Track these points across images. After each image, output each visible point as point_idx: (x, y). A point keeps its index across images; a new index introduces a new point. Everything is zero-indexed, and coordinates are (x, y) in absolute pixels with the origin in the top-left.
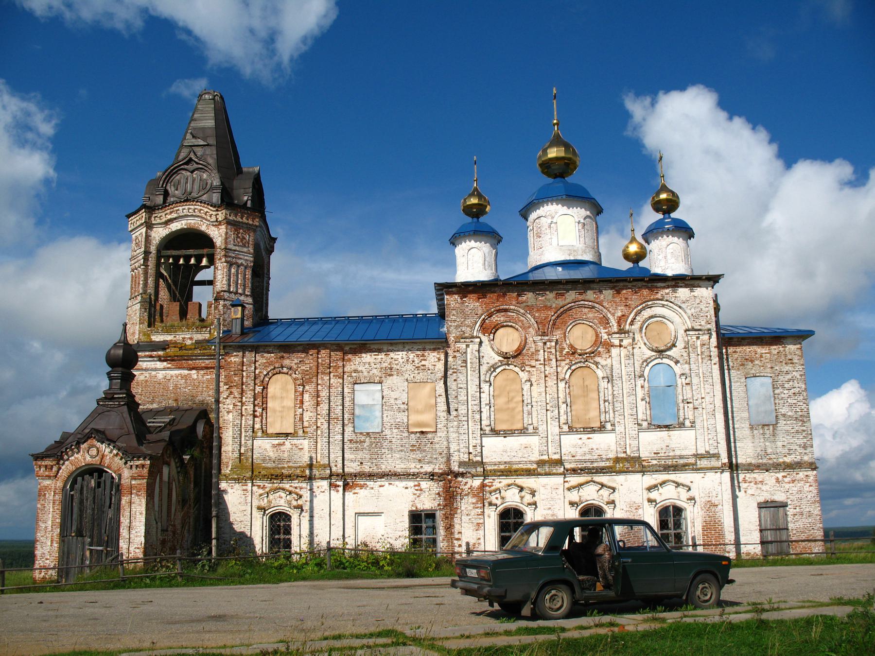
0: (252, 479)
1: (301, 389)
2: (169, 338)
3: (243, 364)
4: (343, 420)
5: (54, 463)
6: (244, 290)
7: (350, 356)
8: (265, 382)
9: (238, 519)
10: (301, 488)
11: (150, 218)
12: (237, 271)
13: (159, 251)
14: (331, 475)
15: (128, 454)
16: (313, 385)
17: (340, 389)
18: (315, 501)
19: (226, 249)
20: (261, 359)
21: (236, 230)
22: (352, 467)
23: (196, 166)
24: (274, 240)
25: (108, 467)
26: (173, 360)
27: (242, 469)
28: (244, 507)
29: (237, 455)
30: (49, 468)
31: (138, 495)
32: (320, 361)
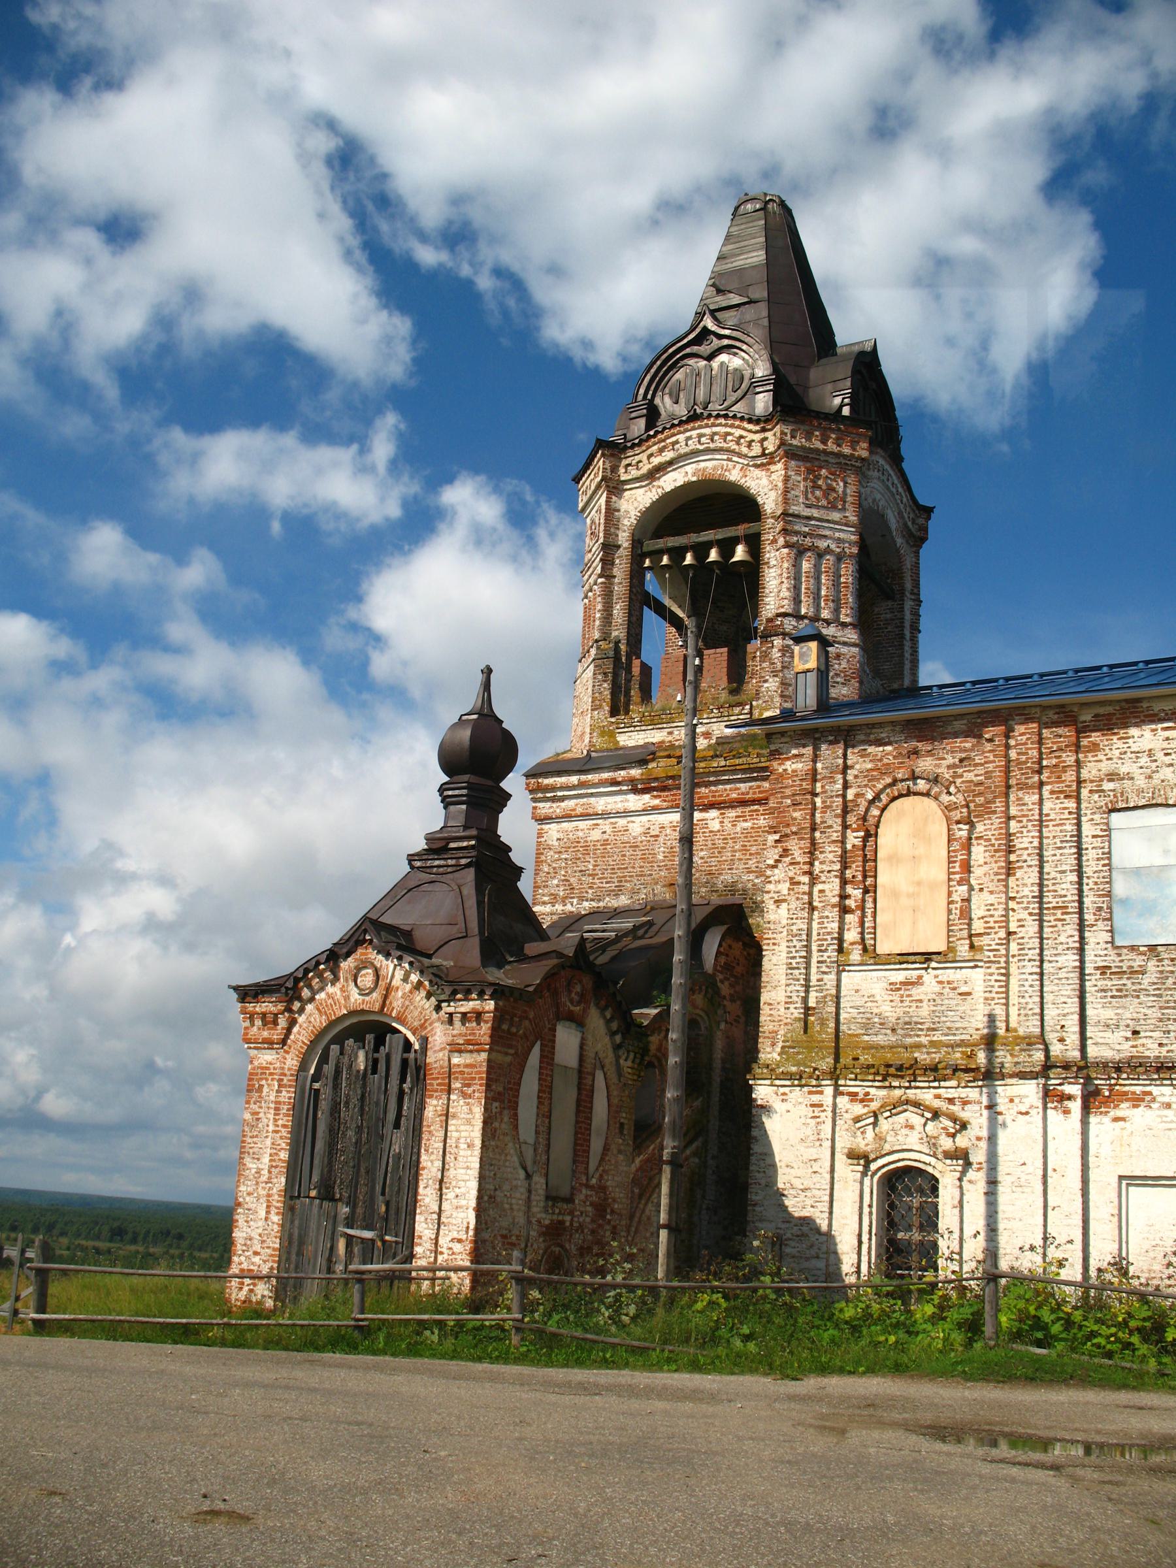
0: (834, 1075)
1: (962, 832)
2: (656, 736)
3: (814, 776)
4: (1081, 912)
5: (281, 1007)
6: (837, 611)
7: (1095, 737)
8: (871, 821)
9: (797, 1183)
10: (965, 1103)
11: (614, 469)
12: (817, 567)
13: (636, 542)
14: (1048, 1066)
15: (446, 985)
16: (997, 820)
17: (1070, 827)
18: (1003, 1137)
19: (785, 514)
20: (860, 762)
21: (812, 474)
22: (1107, 1045)
23: (717, 343)
24: (928, 511)
25: (399, 1019)
26: (664, 789)
27: (810, 1049)
28: (814, 1154)
29: (796, 1012)
30: (269, 1020)
31: (465, 1095)
32: (1013, 754)
